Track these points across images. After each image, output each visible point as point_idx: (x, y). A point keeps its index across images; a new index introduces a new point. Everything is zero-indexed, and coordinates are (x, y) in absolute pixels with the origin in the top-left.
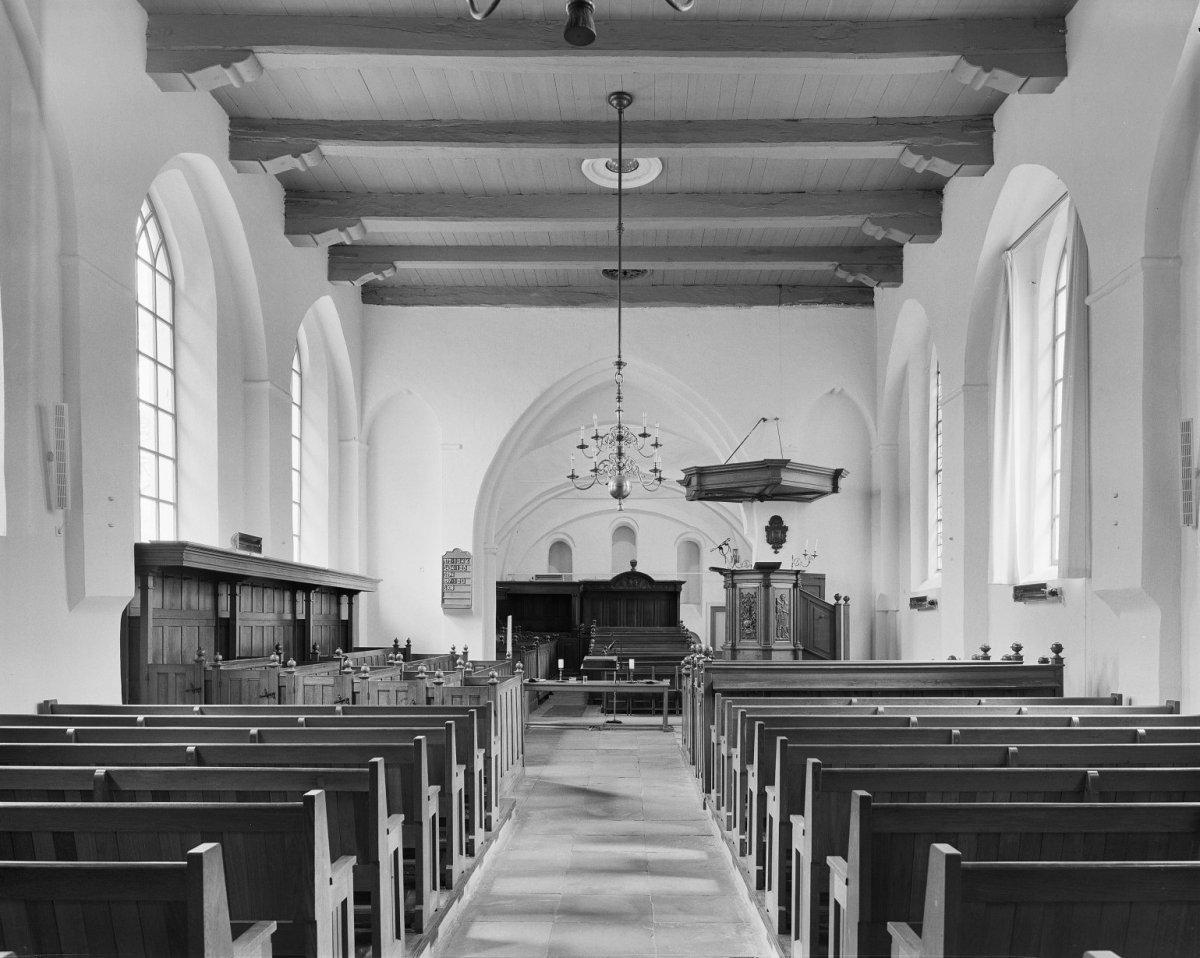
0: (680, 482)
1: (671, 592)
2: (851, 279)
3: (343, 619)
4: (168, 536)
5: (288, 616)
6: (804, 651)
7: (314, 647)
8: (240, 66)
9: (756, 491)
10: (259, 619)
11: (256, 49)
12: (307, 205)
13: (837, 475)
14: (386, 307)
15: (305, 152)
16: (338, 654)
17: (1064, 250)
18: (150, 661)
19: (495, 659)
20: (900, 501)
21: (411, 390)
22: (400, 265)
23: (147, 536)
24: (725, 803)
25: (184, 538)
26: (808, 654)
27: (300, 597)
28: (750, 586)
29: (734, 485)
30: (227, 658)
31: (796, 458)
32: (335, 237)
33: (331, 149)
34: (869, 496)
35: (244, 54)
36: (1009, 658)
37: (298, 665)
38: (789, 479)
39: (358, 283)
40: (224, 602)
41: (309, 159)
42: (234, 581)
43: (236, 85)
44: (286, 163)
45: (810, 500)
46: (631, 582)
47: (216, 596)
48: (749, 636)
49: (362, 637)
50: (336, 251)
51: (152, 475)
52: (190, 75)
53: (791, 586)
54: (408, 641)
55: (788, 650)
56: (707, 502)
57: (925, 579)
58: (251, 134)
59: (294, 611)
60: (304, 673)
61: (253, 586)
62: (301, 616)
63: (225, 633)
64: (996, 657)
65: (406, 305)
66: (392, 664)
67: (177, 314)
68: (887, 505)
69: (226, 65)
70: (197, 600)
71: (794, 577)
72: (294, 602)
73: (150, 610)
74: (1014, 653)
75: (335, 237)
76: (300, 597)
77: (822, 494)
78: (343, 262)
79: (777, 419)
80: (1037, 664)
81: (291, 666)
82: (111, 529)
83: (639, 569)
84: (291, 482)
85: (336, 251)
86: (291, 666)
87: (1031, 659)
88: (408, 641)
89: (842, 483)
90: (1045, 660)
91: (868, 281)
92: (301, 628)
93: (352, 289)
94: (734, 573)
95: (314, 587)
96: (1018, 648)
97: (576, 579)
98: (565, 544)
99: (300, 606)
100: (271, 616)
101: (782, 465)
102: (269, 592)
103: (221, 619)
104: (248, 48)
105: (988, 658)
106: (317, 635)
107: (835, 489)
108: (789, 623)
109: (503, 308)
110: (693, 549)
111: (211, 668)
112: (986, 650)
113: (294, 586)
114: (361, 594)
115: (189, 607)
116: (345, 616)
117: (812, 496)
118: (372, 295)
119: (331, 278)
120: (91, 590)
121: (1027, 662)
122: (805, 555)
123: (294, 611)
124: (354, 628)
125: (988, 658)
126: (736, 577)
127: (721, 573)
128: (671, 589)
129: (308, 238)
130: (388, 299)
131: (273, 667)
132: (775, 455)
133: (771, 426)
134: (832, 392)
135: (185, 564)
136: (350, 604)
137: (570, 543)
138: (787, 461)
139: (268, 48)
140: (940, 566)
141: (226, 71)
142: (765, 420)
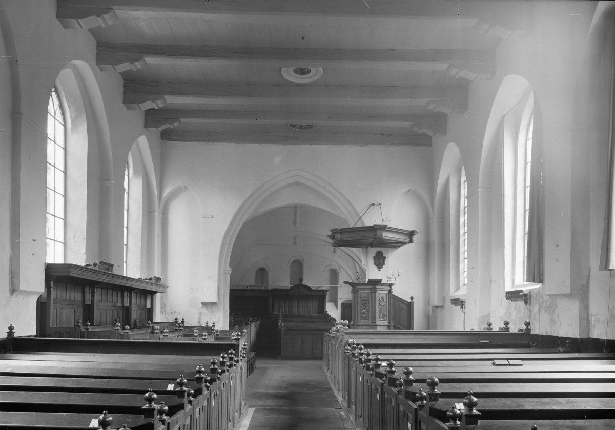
0: (328, 236)
1: (320, 297)
2: (420, 132)
3: (148, 307)
4: (59, 260)
5: (120, 305)
6: (394, 326)
7: (135, 321)
8: (106, 16)
9: (369, 241)
10: (104, 304)
11: (115, 7)
12: (135, 88)
13: (411, 234)
14: (174, 142)
15: (137, 61)
16: (149, 324)
17: (531, 119)
18: (51, 326)
19: (228, 329)
20: (444, 246)
21: (187, 186)
22: (183, 120)
23: (50, 260)
24: (195, 421)
25: (69, 262)
26: (395, 327)
27: (126, 294)
28: (364, 292)
29: (358, 238)
30: (92, 325)
31: (391, 225)
32: (148, 105)
33: (150, 60)
34: (428, 246)
35: (108, 10)
36: (502, 329)
37: (130, 329)
38: (386, 235)
39: (160, 129)
40: (88, 296)
41: (138, 65)
42: (93, 284)
43: (103, 26)
44: (125, 67)
45: (397, 247)
46: (300, 290)
47: (84, 293)
48: (365, 318)
49: (158, 317)
50: (149, 113)
51: (55, 228)
52: (80, 21)
53: (387, 292)
54: (183, 319)
55: (385, 326)
56: (343, 248)
57: (458, 289)
58: (107, 51)
59: (123, 303)
60: (134, 333)
61: (102, 288)
62: (127, 305)
63: (88, 312)
64: (495, 328)
65: (185, 141)
66: (177, 330)
67: (68, 144)
68: (436, 248)
69: (99, 16)
70: (76, 296)
71: (389, 288)
72: (123, 296)
73: (52, 299)
74: (525, 327)
75: (148, 105)
76: (126, 294)
77: (403, 244)
78: (152, 118)
79: (380, 204)
80: (518, 332)
81: (127, 329)
82: (214, 215)
83: (17, 334)
84: (123, 231)
85: (149, 113)
86: (127, 329)
87: (513, 329)
88: (183, 319)
89: (414, 238)
90: (522, 330)
91: (430, 134)
92: (127, 311)
93: (155, 131)
94: (357, 285)
95: (133, 289)
96: (528, 324)
97: (270, 288)
98: (264, 269)
99: (126, 300)
100: (111, 304)
101: (384, 228)
102: (110, 292)
103: (86, 305)
104: (110, 7)
105: (491, 329)
106: (135, 315)
107: (411, 241)
108: (386, 312)
109: (236, 144)
110: (334, 274)
111: (84, 330)
112: (490, 325)
113: (124, 288)
114: (158, 294)
115: (70, 298)
116: (149, 306)
117: (398, 245)
118: (167, 136)
119: (145, 126)
120: (23, 286)
121: (511, 331)
122: (393, 275)
123: (123, 303)
124: (154, 311)
125: (491, 329)
126: (358, 287)
127: (350, 285)
128: (322, 294)
129: (135, 105)
130: (175, 138)
131: (117, 329)
132: (379, 223)
133: (376, 208)
134: (409, 191)
135: (71, 275)
136: (152, 300)
137: (267, 269)
138: (386, 226)
139: (122, 7)
140: (466, 283)
141: (98, 19)
142: (373, 204)
